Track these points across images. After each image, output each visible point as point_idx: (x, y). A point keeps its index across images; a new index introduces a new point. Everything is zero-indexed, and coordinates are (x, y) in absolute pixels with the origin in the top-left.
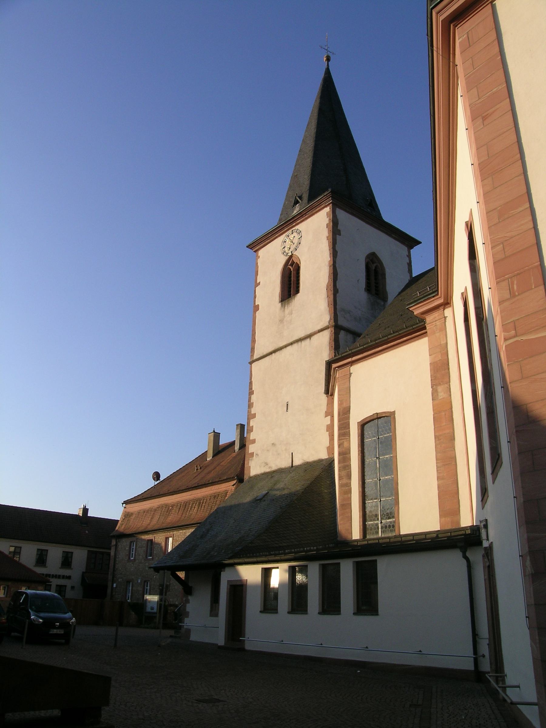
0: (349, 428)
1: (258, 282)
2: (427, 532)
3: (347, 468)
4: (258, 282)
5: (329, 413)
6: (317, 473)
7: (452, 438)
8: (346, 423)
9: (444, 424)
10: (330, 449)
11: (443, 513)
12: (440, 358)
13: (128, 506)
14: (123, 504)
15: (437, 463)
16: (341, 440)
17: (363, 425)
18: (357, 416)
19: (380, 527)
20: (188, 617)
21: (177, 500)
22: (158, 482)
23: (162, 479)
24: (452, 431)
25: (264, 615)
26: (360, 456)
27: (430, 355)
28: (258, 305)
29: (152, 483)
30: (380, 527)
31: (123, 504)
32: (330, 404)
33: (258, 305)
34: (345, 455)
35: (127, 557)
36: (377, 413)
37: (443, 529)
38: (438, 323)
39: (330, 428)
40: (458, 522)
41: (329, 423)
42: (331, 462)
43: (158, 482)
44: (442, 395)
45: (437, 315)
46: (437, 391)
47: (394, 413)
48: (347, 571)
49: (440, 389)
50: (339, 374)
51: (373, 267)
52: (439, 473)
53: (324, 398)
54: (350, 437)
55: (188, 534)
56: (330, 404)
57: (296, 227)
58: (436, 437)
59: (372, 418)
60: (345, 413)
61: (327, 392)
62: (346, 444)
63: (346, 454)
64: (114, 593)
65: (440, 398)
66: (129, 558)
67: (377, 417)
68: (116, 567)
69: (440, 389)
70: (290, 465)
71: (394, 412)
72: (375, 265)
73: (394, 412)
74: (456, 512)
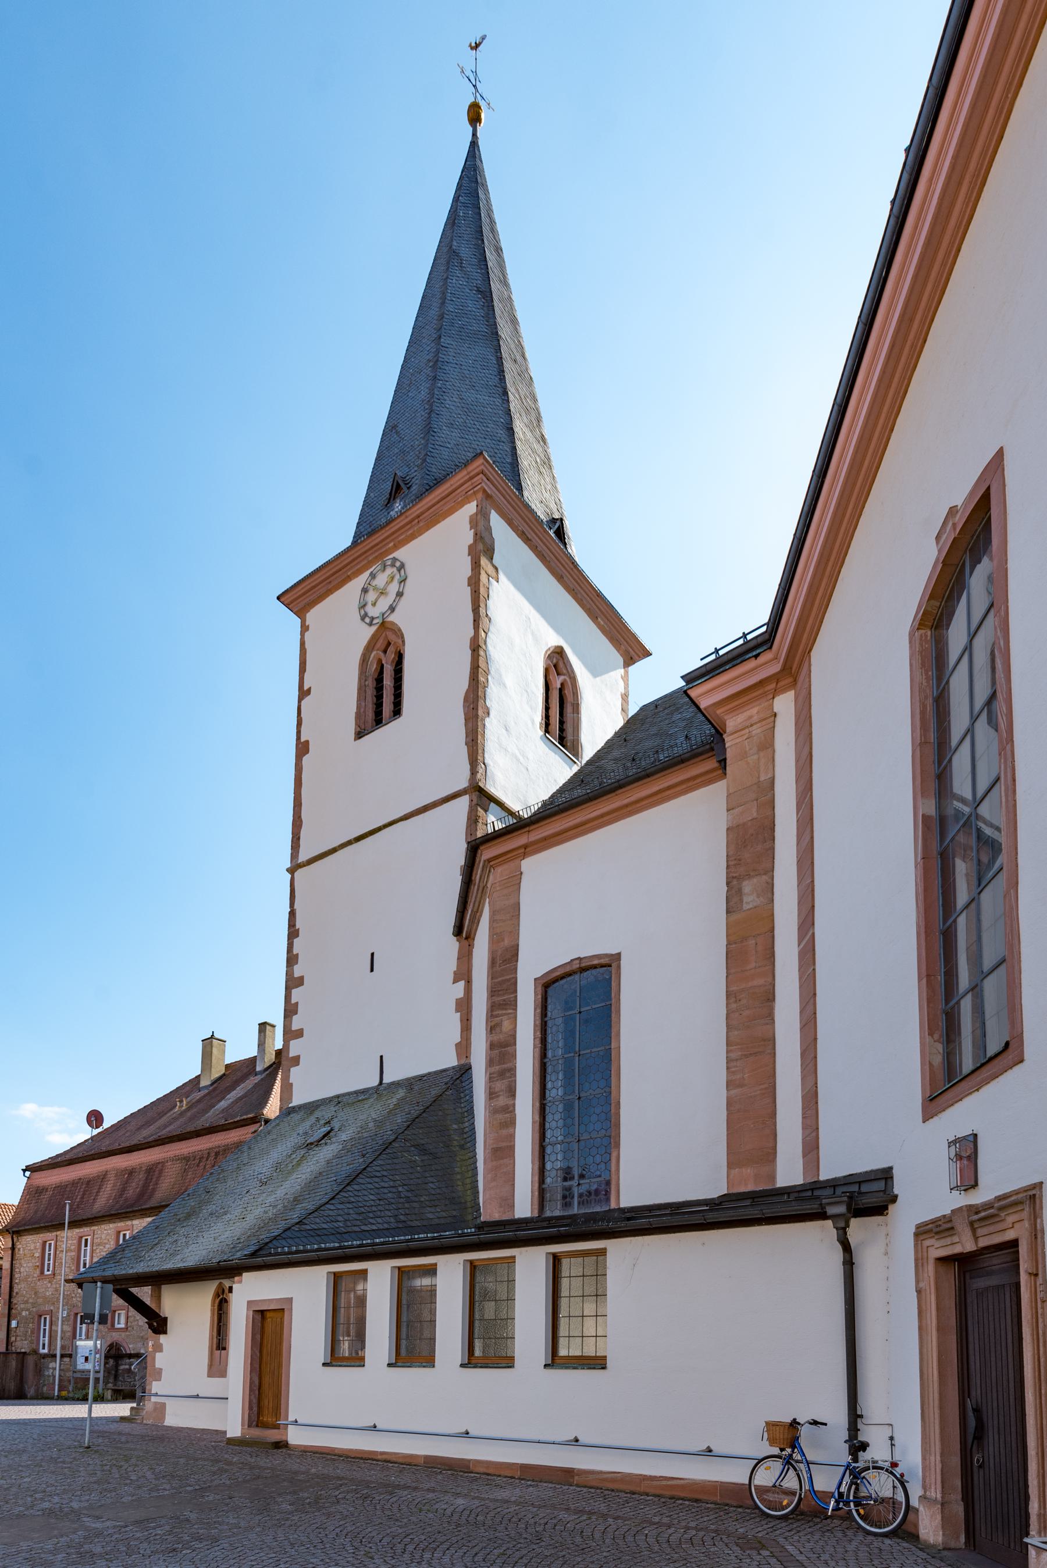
0: (516, 991)
1: (306, 688)
2: (680, 1203)
3: (508, 1075)
4: (306, 688)
5: (464, 974)
6: (435, 1092)
7: (770, 997)
8: (508, 980)
9: (753, 965)
10: (464, 1047)
11: (734, 1161)
12: (755, 815)
13: (37, 1175)
14: (24, 1171)
15: (727, 1052)
16: (497, 1016)
17: (547, 985)
18: (531, 969)
19: (576, 1195)
20: (159, 1379)
21: (138, 1161)
22: (100, 1130)
23: (106, 1125)
24: (770, 979)
25: (289, 1296)
26: (538, 1050)
27: (728, 810)
28: (307, 742)
29: (84, 1133)
30: (576, 1195)
31: (24, 1171)
32: (465, 957)
33: (307, 742)
34: (502, 1051)
35: (38, 1272)
36: (579, 958)
37: (735, 1191)
38: (756, 730)
39: (464, 1006)
40: (773, 1177)
41: (461, 994)
42: (464, 1071)
43: (100, 1130)
44: (750, 900)
45: (755, 711)
46: (740, 891)
47: (618, 957)
48: (450, 1276)
49: (747, 886)
50: (497, 876)
51: (557, 682)
52: (733, 1072)
53: (452, 945)
54: (516, 1010)
55: (145, 1224)
56: (465, 957)
57: (395, 555)
58: (729, 995)
59: (568, 969)
60: (504, 961)
61: (458, 931)
62: (506, 1025)
63: (507, 1045)
64: (13, 1339)
65: (746, 907)
66: (42, 1272)
67: (582, 968)
68: (15, 1290)
69: (747, 886)
70: (376, 1082)
71: (619, 954)
72: (562, 678)
73: (619, 954)
74: (770, 1155)
